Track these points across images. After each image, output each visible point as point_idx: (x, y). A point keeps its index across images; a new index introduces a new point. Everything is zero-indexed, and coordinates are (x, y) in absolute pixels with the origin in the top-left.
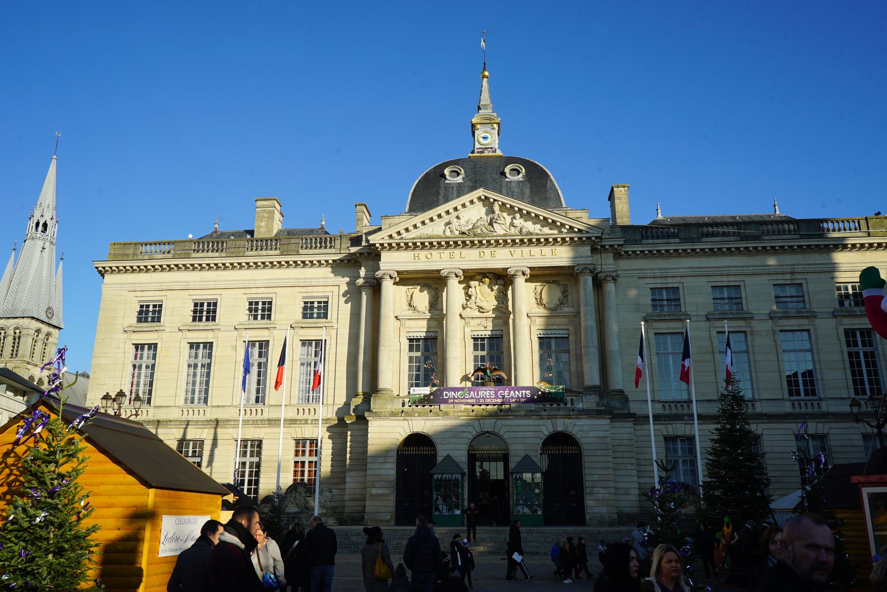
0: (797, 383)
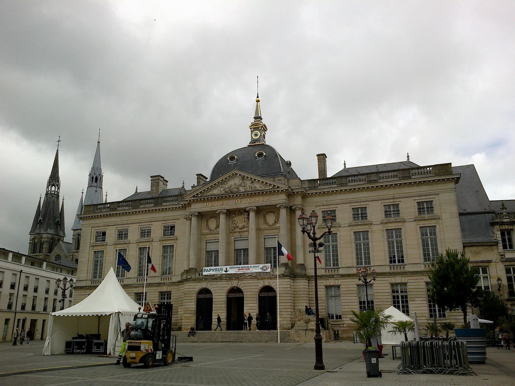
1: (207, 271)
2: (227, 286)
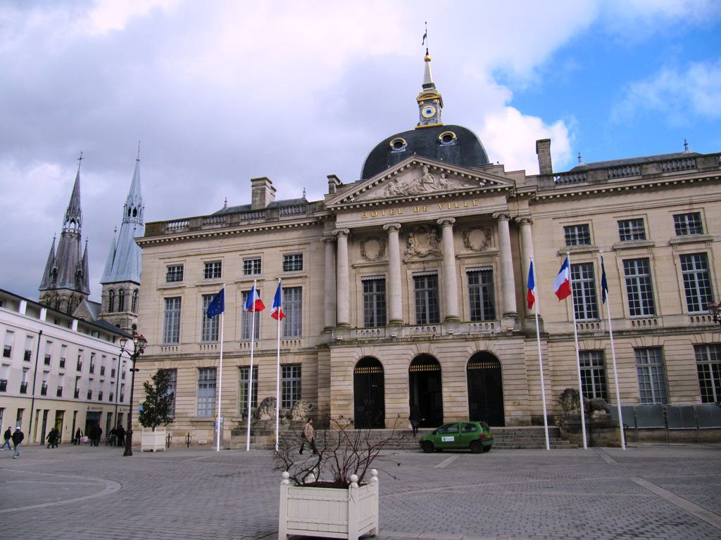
0: (486, 311)
2: (410, 352)
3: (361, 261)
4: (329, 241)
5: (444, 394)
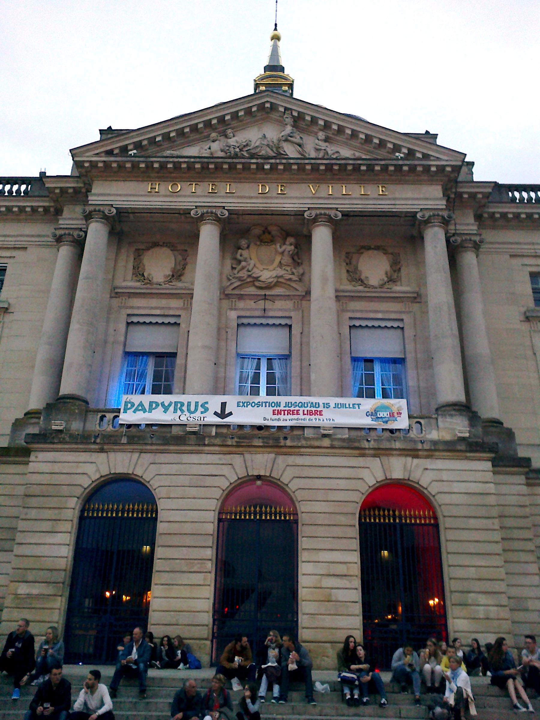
1: (141, 407)
2: (226, 470)
3: (131, 283)
4: (70, 238)
5: (303, 581)
